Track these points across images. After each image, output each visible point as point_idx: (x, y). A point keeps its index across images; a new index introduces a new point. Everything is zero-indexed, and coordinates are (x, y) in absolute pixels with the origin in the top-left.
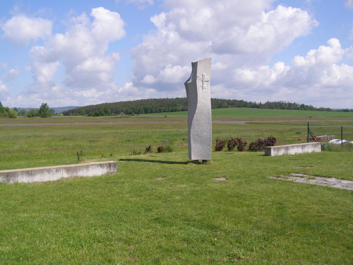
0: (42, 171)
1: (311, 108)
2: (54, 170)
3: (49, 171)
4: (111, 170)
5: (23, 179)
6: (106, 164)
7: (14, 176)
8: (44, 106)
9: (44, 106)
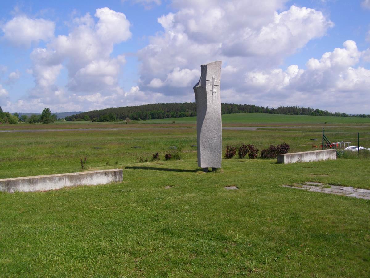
0: (44, 180)
1: (326, 114)
2: (57, 179)
3: (51, 179)
4: (116, 178)
5: (25, 188)
6: (111, 172)
7: (15, 185)
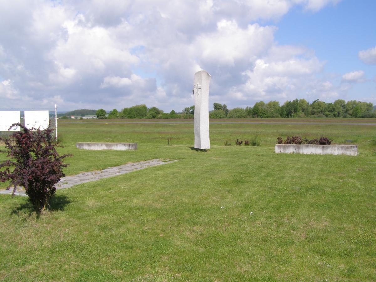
0: (94, 145)
1: (155, 114)
2: (100, 145)
3: (98, 145)
4: (130, 148)
5: (86, 148)
6: (127, 144)
7: (83, 146)
8: (173, 112)
9: (173, 112)
